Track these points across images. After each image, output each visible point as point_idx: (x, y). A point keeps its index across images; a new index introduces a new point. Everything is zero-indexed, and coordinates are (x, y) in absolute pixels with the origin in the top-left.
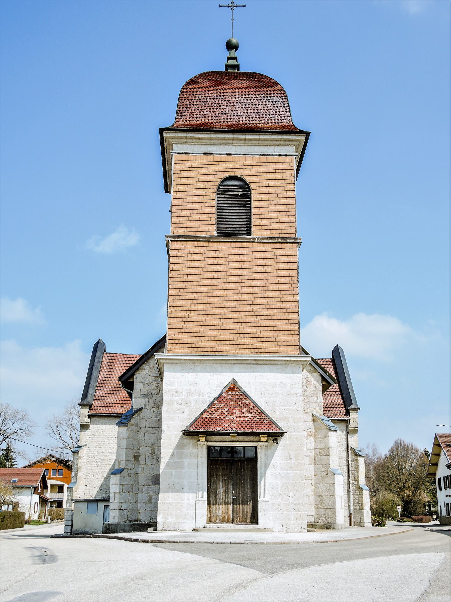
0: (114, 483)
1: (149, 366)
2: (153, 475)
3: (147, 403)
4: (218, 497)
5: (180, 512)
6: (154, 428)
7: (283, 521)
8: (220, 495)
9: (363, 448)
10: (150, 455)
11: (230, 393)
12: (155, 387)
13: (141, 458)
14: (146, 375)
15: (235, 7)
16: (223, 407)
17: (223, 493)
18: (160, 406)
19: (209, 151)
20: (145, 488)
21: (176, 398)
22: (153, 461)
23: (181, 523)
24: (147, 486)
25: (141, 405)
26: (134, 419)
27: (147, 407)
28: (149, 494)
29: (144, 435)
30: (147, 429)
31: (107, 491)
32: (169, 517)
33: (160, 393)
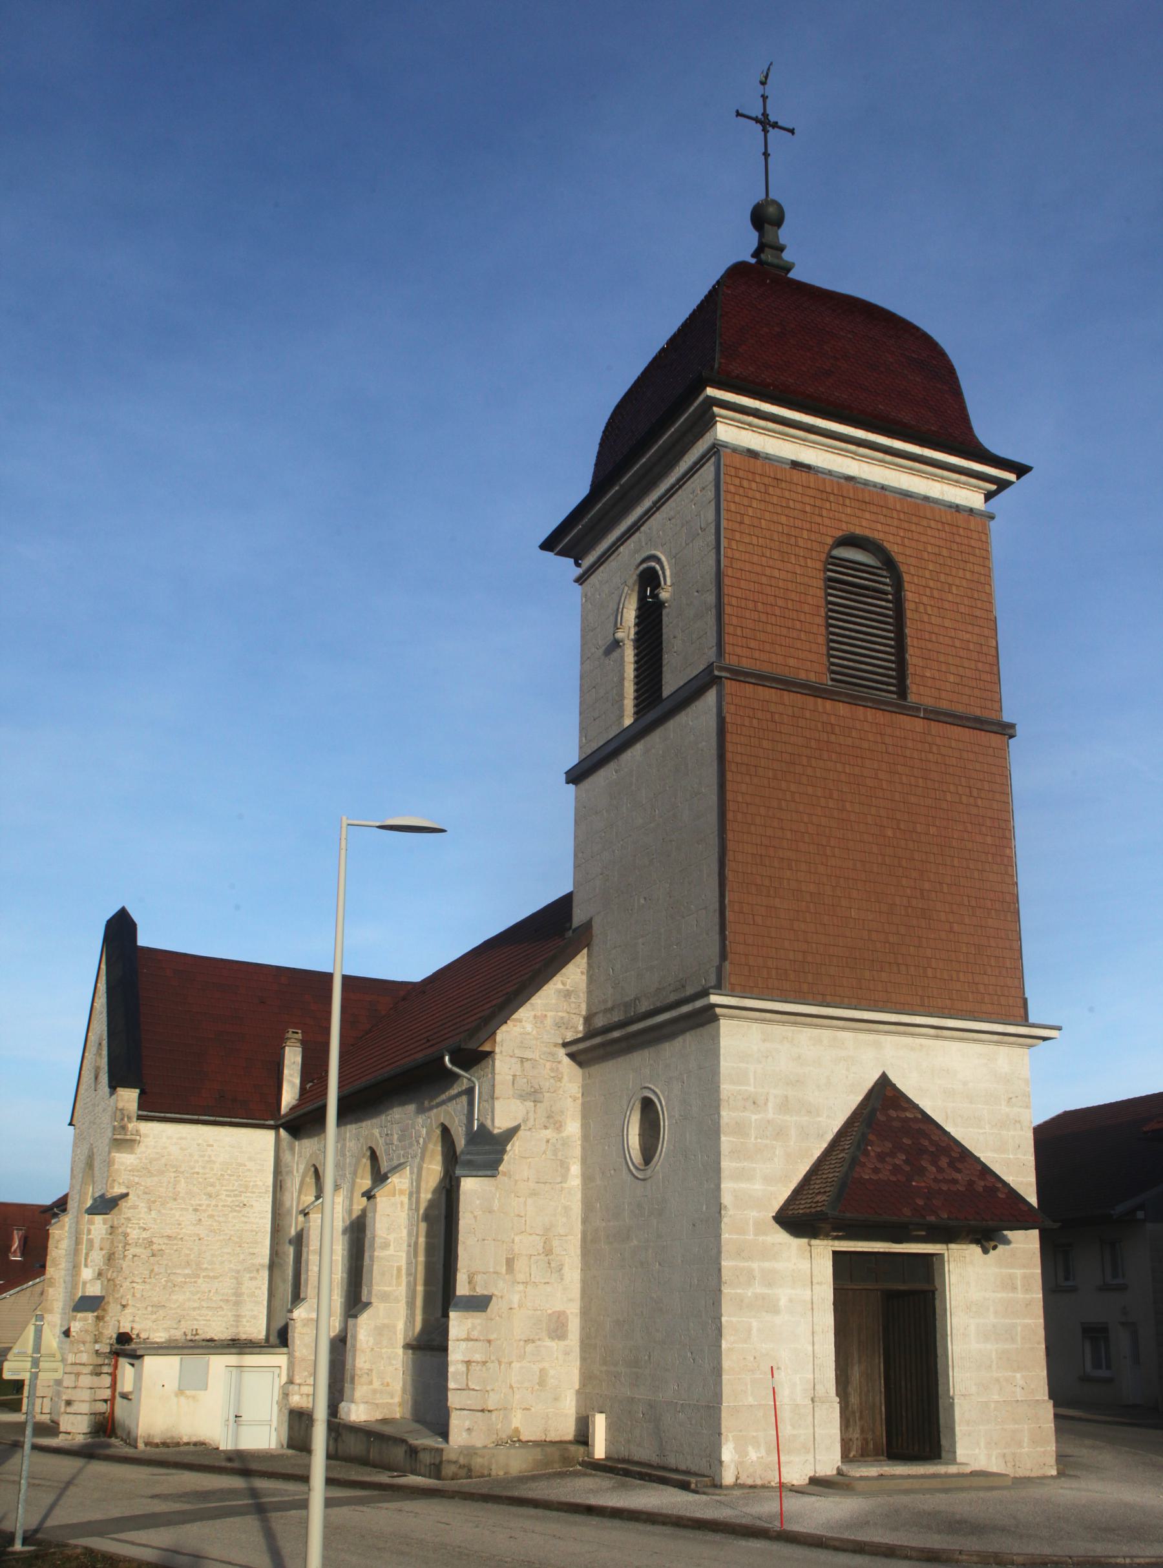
0: (463, 1335)
1: (533, 1013)
2: (549, 1312)
3: (531, 1115)
6: (550, 1183)
10: (542, 1257)
12: (549, 1072)
14: (528, 1037)
20: (530, 1347)
21: (754, 1117)
24: (533, 1341)
27: (530, 1123)
29: (525, 1202)
31: (180, 1321)
33: (561, 1089)
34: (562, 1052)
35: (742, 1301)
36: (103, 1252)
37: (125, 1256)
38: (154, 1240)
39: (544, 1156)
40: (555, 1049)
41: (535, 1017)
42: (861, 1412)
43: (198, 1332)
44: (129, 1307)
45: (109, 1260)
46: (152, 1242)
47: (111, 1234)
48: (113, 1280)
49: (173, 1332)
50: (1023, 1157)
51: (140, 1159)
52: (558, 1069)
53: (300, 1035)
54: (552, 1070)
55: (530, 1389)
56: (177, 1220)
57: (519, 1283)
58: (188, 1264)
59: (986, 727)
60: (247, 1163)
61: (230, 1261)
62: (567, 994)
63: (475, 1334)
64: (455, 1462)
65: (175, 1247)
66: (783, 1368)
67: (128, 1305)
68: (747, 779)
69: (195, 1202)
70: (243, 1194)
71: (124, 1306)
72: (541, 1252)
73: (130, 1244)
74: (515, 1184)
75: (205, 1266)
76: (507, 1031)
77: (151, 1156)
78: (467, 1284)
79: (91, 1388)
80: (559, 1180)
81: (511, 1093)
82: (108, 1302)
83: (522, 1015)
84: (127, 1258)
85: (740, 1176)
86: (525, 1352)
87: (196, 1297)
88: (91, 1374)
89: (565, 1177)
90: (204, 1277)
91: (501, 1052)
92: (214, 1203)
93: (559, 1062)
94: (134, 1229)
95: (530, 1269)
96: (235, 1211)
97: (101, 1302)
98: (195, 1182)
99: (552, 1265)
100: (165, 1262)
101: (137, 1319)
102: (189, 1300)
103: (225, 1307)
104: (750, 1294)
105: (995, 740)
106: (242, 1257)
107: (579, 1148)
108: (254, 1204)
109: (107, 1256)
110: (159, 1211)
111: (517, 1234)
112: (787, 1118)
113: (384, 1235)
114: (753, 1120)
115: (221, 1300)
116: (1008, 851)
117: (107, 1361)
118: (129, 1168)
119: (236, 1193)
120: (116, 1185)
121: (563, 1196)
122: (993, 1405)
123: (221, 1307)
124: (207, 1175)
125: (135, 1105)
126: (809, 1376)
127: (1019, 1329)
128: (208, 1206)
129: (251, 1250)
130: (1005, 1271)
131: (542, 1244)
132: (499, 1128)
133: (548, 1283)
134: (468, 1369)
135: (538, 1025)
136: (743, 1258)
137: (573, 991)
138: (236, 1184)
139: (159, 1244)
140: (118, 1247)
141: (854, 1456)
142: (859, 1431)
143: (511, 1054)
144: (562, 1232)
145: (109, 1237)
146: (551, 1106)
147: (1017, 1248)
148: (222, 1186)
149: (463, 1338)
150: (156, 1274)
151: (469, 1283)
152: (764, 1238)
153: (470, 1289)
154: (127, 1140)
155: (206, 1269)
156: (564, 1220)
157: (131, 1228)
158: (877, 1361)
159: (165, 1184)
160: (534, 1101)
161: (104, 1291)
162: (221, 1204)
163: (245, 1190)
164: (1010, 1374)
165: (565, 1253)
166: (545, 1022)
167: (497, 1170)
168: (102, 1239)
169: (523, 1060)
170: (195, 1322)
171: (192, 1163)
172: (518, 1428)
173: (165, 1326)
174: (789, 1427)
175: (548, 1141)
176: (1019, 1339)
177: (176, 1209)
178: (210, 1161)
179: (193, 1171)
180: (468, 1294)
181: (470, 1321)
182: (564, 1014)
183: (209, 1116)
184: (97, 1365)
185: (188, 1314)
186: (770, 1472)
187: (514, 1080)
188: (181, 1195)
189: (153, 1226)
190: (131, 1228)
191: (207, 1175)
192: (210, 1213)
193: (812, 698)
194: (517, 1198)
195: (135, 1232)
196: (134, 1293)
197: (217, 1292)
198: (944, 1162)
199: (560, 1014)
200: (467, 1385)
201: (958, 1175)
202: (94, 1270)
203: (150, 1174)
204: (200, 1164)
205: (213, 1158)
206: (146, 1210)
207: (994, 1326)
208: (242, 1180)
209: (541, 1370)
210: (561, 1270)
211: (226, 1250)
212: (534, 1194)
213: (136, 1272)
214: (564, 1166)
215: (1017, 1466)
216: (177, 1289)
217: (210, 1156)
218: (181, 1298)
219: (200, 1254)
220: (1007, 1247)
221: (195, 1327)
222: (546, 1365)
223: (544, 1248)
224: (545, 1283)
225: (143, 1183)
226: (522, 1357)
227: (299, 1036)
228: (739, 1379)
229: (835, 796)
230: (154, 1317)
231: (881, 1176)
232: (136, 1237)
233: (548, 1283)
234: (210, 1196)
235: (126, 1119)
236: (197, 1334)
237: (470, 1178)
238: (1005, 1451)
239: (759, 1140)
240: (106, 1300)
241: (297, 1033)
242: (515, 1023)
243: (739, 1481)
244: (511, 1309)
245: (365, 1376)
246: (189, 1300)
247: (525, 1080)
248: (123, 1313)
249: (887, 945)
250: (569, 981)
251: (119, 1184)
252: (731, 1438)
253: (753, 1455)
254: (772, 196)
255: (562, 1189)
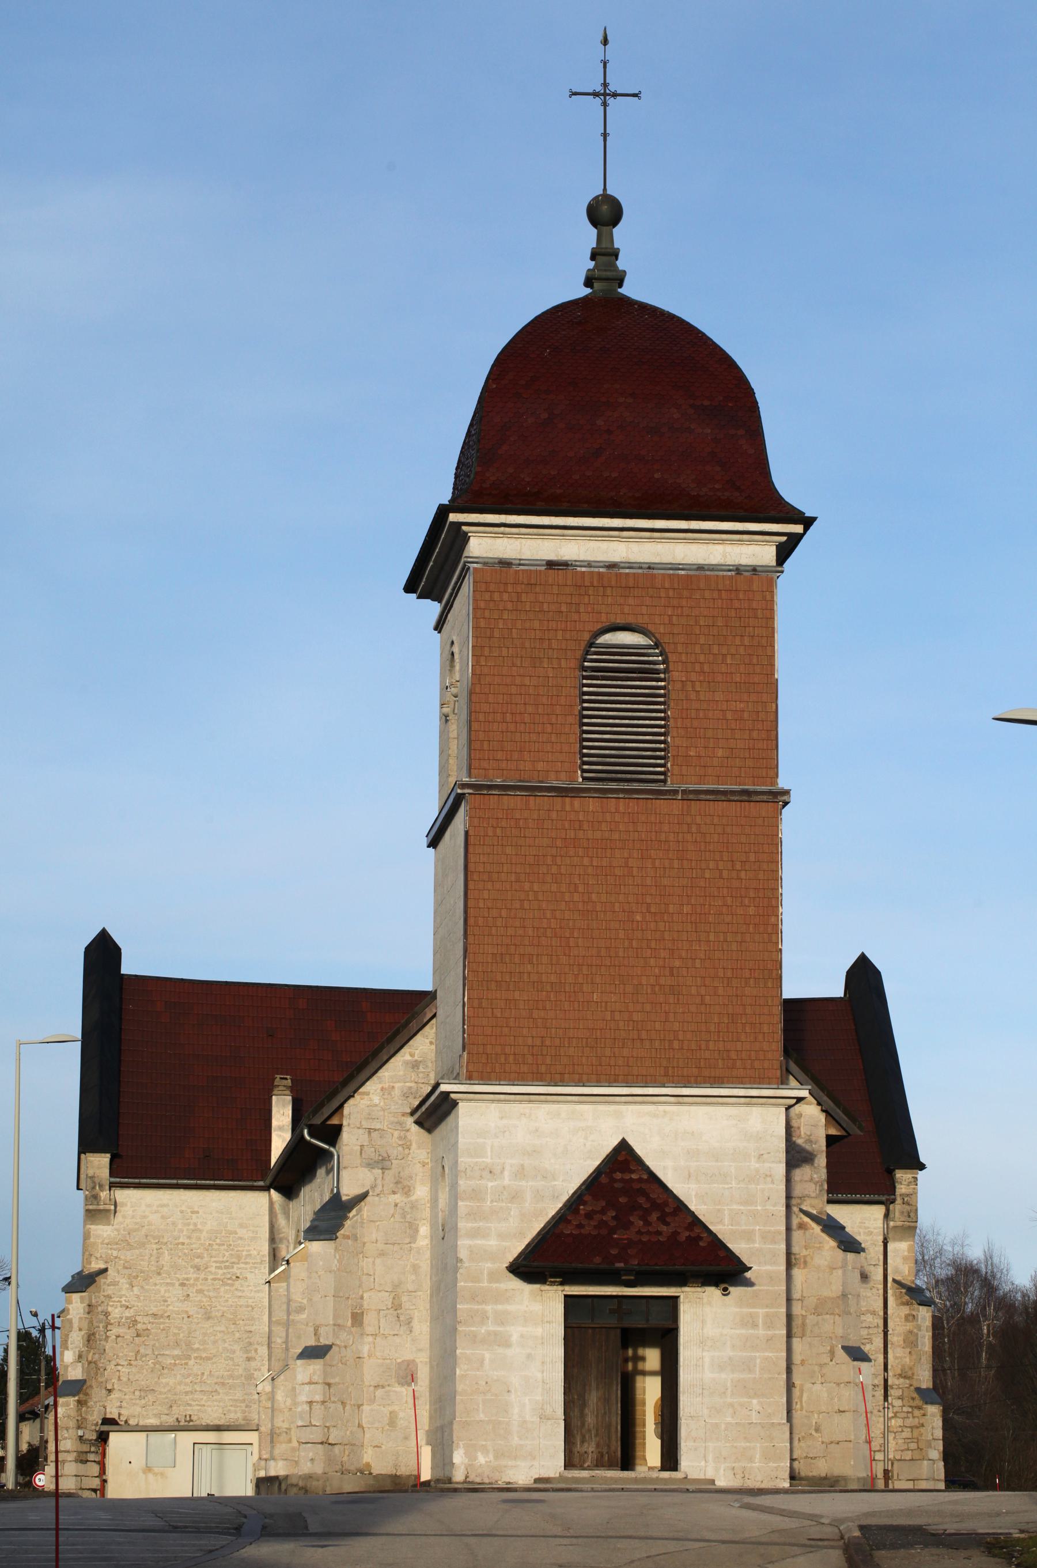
0: (307, 1380)
1: (380, 1086)
2: (399, 1361)
3: (379, 1182)
4: (586, 1411)
5: (502, 1443)
6: (399, 1244)
7: (735, 1462)
8: (592, 1408)
9: (801, 1115)
10: (391, 1311)
11: (618, 1175)
12: (397, 1140)
13: (367, 1319)
15: (613, 96)
16: (603, 1212)
17: (599, 1404)
18: (412, 1188)
19: (1024, 1495)
20: (379, 1392)
21: (490, 1184)
22: (398, 1326)
23: (505, 1467)
24: (383, 1387)
25: (363, 1185)
26: (348, 1221)
28: (390, 1409)
29: (374, 1262)
30: (380, 1246)
31: (171, 1407)
32: (479, 1454)
33: (410, 1156)
34: (410, 1120)
35: (475, 1336)
36: (83, 1333)
37: (107, 1337)
38: (138, 1318)
39: (392, 1219)
40: (403, 1118)
41: (382, 1089)
42: (597, 1430)
43: (192, 1418)
44: (114, 1392)
45: (88, 1341)
46: (136, 1321)
47: (89, 1313)
48: (95, 1363)
49: (164, 1418)
50: (772, 1208)
51: (118, 1230)
52: (406, 1137)
53: (289, 1081)
54: (400, 1138)
55: (380, 1429)
56: (162, 1297)
57: (368, 1335)
58: (177, 1344)
59: (755, 798)
60: (238, 1230)
61: (224, 1341)
62: (415, 1065)
63: (315, 1378)
64: (296, 1485)
65: (162, 1327)
66: (513, 1391)
67: (114, 1389)
68: (489, 885)
69: (181, 1276)
70: (235, 1266)
71: (110, 1391)
72: (390, 1307)
73: (112, 1324)
74: (364, 1246)
75: (196, 1346)
76: (354, 1105)
77: (130, 1226)
78: (313, 1335)
79: (76, 1476)
80: (407, 1240)
81: (359, 1161)
82: (91, 1386)
83: (369, 1088)
84: (110, 1339)
85: (475, 1233)
86: (375, 1396)
87: (188, 1380)
88: (76, 1461)
89: (413, 1238)
90: (196, 1358)
91: (349, 1125)
92: (202, 1276)
93: (408, 1130)
94: (116, 1308)
95: (379, 1323)
96: (228, 1284)
97: (83, 1386)
98: (180, 1254)
99: (401, 1319)
100: (152, 1343)
101: (124, 1404)
102: (180, 1383)
103: (221, 1391)
104: (483, 1331)
105: (765, 809)
106: (237, 1335)
107: (428, 1210)
108: (248, 1275)
109: (86, 1336)
110: (142, 1287)
111: (366, 1291)
112: (523, 1183)
113: (300, 1300)
114: (489, 1186)
115: (216, 1383)
116: (773, 919)
117: (93, 1449)
118: (106, 1241)
119: (227, 1264)
120: (93, 1259)
121: (412, 1255)
122: (723, 1426)
123: (216, 1391)
124: (194, 1246)
125: (106, 1172)
126: (538, 1398)
127: (758, 1361)
128: (197, 1279)
129: (248, 1328)
130: (745, 1310)
131: (391, 1300)
132: (347, 1195)
133: (397, 1335)
134: (311, 1409)
135: (385, 1097)
136: (478, 1302)
137: (420, 1062)
138: (227, 1254)
139: (144, 1323)
140: (99, 1327)
141: (588, 1466)
142: (595, 1446)
143: (359, 1126)
144: (411, 1287)
145: (87, 1316)
146: (399, 1173)
147: (760, 1290)
148: (211, 1257)
149: (306, 1382)
150: (142, 1356)
151: (315, 1335)
152: (497, 1285)
153: (316, 1341)
154: (100, 1211)
155: (198, 1349)
156: (413, 1277)
157: (112, 1306)
158: (614, 1388)
159: (146, 1258)
160: (382, 1169)
161: (85, 1374)
162: (210, 1277)
163: (237, 1261)
164: (746, 1400)
165: (414, 1307)
166: (393, 1093)
167: (335, 1234)
168: (80, 1318)
169: (370, 1131)
170: (189, 1408)
171: (176, 1233)
172: (369, 1463)
173: (155, 1412)
174: (516, 1438)
175: (396, 1205)
176: (757, 1369)
177: (161, 1284)
178: (195, 1230)
179: (177, 1241)
180: (314, 1344)
181: (311, 1367)
182: (413, 1085)
183: (188, 1179)
184: (81, 1452)
185: (180, 1399)
186: (498, 1473)
187: (361, 1150)
188: (165, 1268)
189: (136, 1303)
190: (112, 1306)
191: (194, 1246)
192: (200, 1287)
193: (559, 799)
194: (365, 1259)
195: (117, 1311)
196: (119, 1377)
197: (211, 1374)
198: (654, 1217)
199: (408, 1084)
200: (310, 1422)
201: (665, 1227)
202: (74, 1352)
203: (130, 1246)
204: (184, 1233)
205: (199, 1226)
206: (128, 1286)
207: (730, 1358)
208: (233, 1250)
209: (391, 1413)
210: (409, 1323)
211: (218, 1328)
212: (382, 1254)
213: (121, 1354)
214: (413, 1229)
215: (746, 1478)
216: (166, 1371)
217: (195, 1224)
218: (172, 1381)
219: (190, 1333)
220: (749, 1288)
221: (188, 1413)
222: (396, 1408)
223: (393, 1303)
224: (394, 1335)
225: (122, 1257)
226: (372, 1401)
227: (289, 1082)
228: (471, 1399)
229: (581, 889)
230: (143, 1402)
231: (583, 1231)
232: (118, 1316)
233: (397, 1335)
234: (197, 1268)
235: (97, 1188)
236: (191, 1421)
237: (315, 1242)
238: (733, 1465)
239: (495, 1204)
240: (88, 1384)
241: (286, 1079)
242: (362, 1097)
243: (468, 1479)
244: (359, 1358)
245: (284, 1434)
246: (180, 1383)
247: (373, 1149)
248: (108, 1398)
249: (631, 1022)
250: (417, 1052)
251: (97, 1258)
252: (462, 1446)
253: (482, 1459)
254: (609, 192)
255: (411, 1249)
